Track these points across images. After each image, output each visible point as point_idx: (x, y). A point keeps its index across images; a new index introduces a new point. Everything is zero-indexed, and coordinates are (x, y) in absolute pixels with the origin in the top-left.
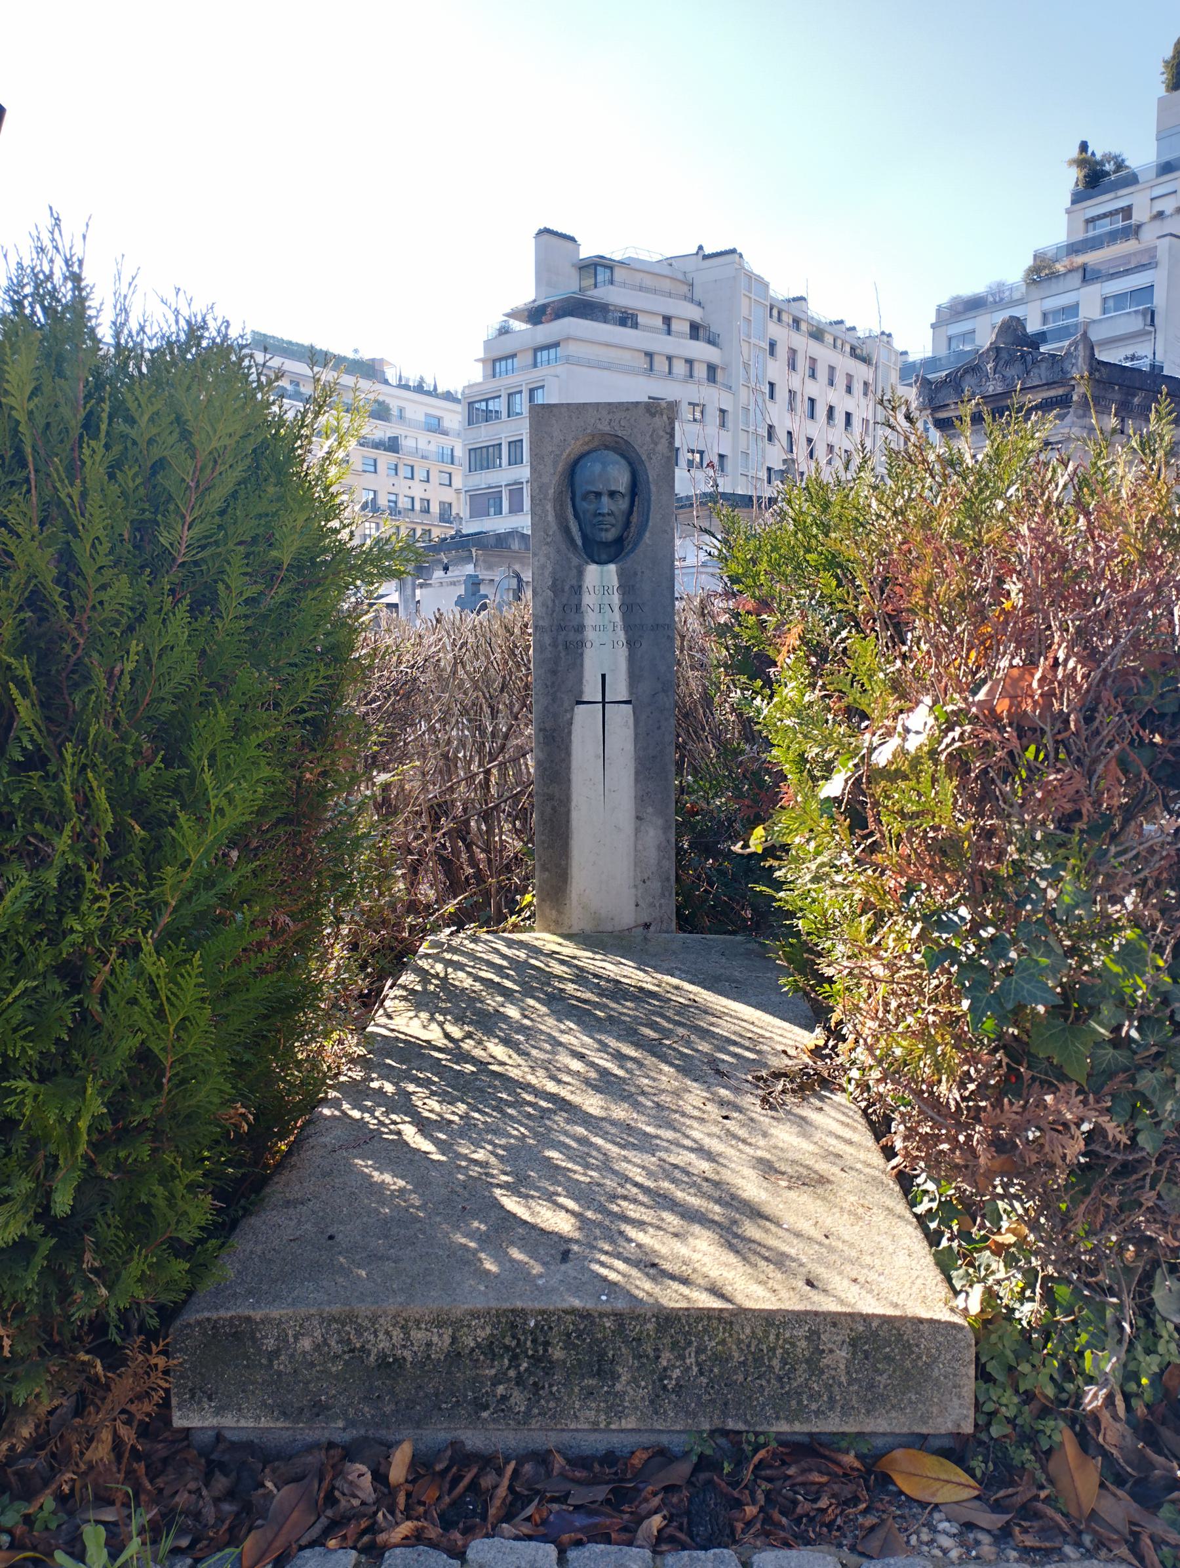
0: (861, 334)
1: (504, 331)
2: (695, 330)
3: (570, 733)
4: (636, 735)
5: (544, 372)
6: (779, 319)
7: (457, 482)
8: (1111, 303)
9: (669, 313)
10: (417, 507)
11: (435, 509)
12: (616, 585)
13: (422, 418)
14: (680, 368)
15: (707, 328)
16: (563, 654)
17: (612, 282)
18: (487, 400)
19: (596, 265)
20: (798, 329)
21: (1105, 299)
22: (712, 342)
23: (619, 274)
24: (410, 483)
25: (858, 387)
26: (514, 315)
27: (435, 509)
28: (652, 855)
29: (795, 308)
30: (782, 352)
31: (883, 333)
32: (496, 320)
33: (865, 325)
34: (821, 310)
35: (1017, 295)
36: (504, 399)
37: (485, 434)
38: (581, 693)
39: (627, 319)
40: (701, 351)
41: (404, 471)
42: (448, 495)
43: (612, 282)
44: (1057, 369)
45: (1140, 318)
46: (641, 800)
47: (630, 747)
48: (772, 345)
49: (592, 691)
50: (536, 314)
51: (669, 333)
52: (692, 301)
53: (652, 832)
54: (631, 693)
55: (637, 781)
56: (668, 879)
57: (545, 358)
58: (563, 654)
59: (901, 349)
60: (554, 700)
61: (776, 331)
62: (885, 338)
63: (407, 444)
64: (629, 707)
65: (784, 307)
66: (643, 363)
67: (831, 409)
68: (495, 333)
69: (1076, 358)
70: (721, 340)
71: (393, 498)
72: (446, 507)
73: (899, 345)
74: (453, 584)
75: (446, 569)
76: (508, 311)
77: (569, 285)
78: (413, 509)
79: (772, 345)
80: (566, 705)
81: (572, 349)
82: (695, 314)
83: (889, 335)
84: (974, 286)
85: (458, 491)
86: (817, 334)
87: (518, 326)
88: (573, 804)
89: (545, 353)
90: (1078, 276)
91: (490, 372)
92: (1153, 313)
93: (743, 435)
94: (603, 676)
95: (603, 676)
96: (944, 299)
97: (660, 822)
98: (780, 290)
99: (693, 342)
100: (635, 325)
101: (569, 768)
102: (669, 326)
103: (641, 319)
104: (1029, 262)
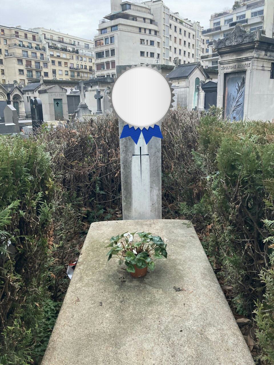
0: (192, 22)
1: (103, 22)
2: (152, 21)
3: (131, 164)
4: (150, 164)
5: (114, 33)
6: (172, 18)
7: (93, 61)
8: (253, 15)
9: (145, 17)
10: (84, 68)
11: (88, 68)
12: (173, 220)
13: (84, 45)
14: (147, 32)
15: (154, 21)
16: (128, 141)
17: (130, 9)
18: (100, 40)
19: (126, 4)
20: (177, 21)
21: (252, 13)
22: (156, 25)
23: (132, 7)
24: (81, 62)
25: (191, 36)
26: (106, 18)
27: (88, 68)
28: (155, 197)
29: (175, 16)
30: (173, 27)
31: (197, 22)
32: (102, 18)
33: (193, 20)
34: (182, 16)
35: (231, 12)
36: (104, 40)
37: (99, 49)
38: (134, 152)
39: (135, 18)
40: (152, 27)
41: (80, 59)
42: (91, 64)
43: (130, 9)
44: (251, 38)
45: (260, 18)
46: (152, 182)
47: (148, 167)
48: (170, 25)
49: (137, 152)
50: (111, 17)
51: (145, 22)
52: (150, 14)
53: (155, 191)
54: (149, 153)
55: (151, 177)
56: (160, 204)
57: (114, 29)
58: (128, 141)
59: (202, 26)
60: (126, 155)
61: (171, 22)
62: (198, 23)
63: (80, 52)
64: (148, 156)
65: (173, 15)
66: (138, 30)
67: (185, 42)
68: (101, 23)
69: (256, 35)
70: (158, 24)
71: (78, 65)
72: (91, 68)
73: (201, 25)
74: (93, 91)
75: (91, 87)
76: (104, 17)
77: (119, 10)
78: (83, 68)
79: (170, 25)
80: (130, 156)
81: (120, 27)
82: (151, 17)
83: (199, 23)
84: (221, 11)
85: (94, 64)
86: (181, 22)
87: (106, 20)
88: (132, 184)
89: (114, 28)
90: (245, 7)
91: (100, 33)
92: (263, 17)
93: (163, 49)
94: (140, 148)
95: (140, 148)
96: (213, 13)
97: (157, 188)
98: (172, 11)
99: (151, 25)
100: (136, 20)
101: (131, 174)
102: (145, 20)
103: (138, 19)
104: (234, 4)
